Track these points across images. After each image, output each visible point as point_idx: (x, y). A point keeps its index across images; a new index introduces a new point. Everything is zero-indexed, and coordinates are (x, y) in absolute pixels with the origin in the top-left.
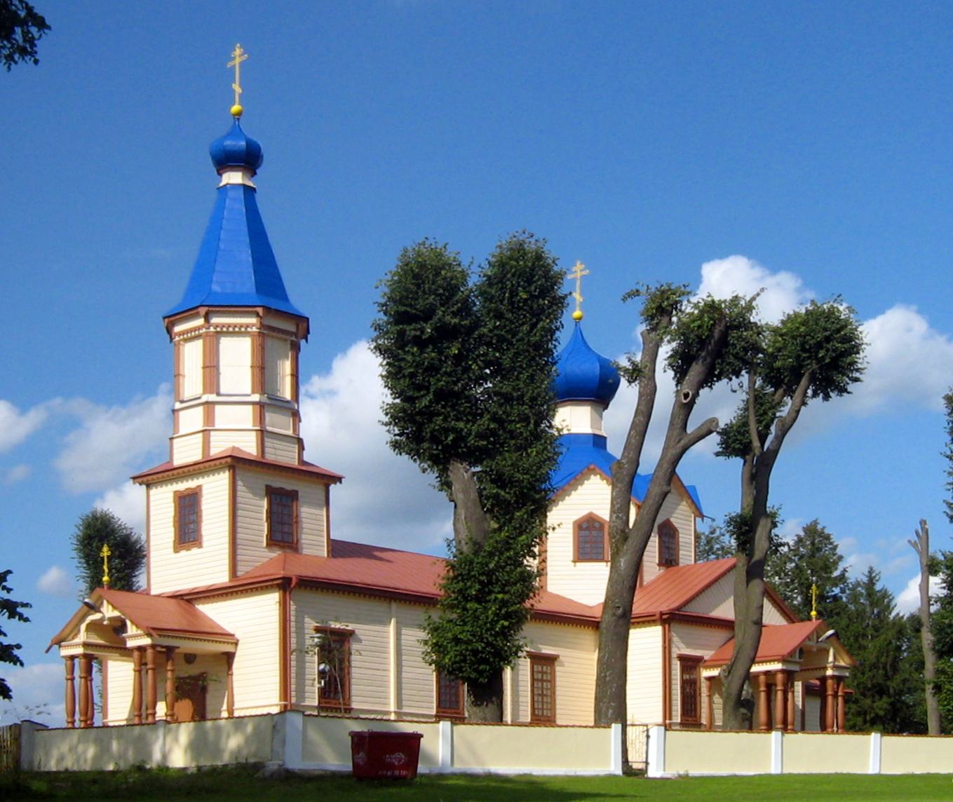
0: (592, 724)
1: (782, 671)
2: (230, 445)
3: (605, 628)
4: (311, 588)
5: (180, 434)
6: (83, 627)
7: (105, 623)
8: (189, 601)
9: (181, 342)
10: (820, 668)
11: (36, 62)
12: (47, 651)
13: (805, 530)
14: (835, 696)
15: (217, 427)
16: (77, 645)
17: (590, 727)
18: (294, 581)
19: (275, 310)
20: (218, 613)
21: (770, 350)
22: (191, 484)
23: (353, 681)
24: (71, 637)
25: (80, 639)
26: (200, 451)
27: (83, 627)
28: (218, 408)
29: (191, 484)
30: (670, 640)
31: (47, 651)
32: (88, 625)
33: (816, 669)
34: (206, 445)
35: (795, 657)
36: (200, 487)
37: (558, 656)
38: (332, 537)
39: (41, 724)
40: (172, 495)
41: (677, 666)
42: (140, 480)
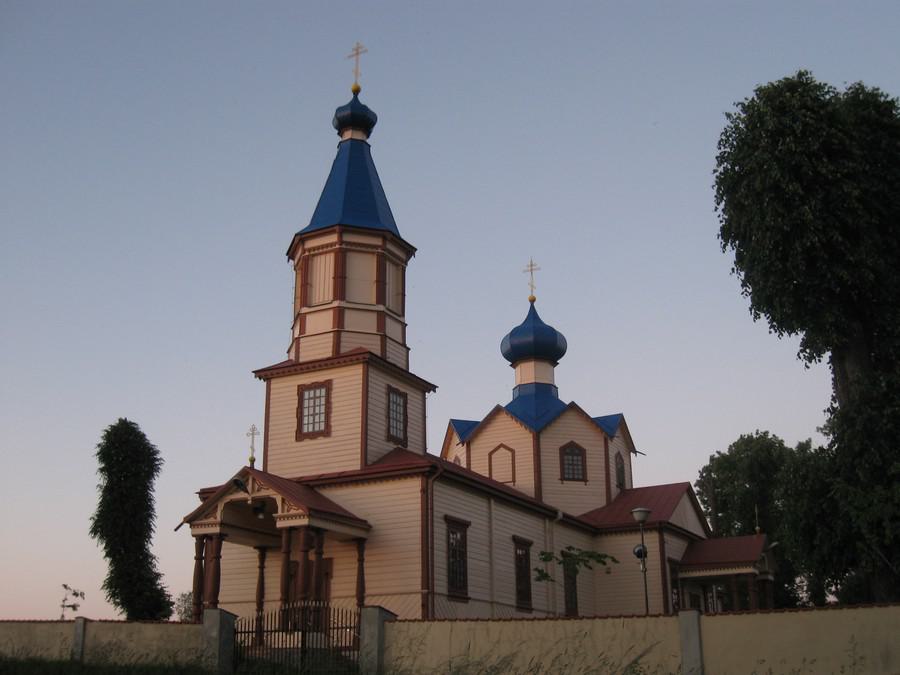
0: (419, 615)
1: (308, 528)
2: (358, 346)
5: (307, 334)
6: (221, 507)
8: (312, 488)
11: (356, 92)
12: (176, 530)
13: (893, 101)
15: (332, 334)
16: (213, 525)
17: (419, 621)
18: (560, 516)
20: (352, 499)
24: (203, 515)
25: (216, 518)
27: (221, 507)
28: (308, 317)
30: (451, 439)
31: (176, 530)
32: (226, 504)
37: (470, 523)
38: (668, 555)
39: (680, 528)
41: (440, 529)
42: (262, 374)
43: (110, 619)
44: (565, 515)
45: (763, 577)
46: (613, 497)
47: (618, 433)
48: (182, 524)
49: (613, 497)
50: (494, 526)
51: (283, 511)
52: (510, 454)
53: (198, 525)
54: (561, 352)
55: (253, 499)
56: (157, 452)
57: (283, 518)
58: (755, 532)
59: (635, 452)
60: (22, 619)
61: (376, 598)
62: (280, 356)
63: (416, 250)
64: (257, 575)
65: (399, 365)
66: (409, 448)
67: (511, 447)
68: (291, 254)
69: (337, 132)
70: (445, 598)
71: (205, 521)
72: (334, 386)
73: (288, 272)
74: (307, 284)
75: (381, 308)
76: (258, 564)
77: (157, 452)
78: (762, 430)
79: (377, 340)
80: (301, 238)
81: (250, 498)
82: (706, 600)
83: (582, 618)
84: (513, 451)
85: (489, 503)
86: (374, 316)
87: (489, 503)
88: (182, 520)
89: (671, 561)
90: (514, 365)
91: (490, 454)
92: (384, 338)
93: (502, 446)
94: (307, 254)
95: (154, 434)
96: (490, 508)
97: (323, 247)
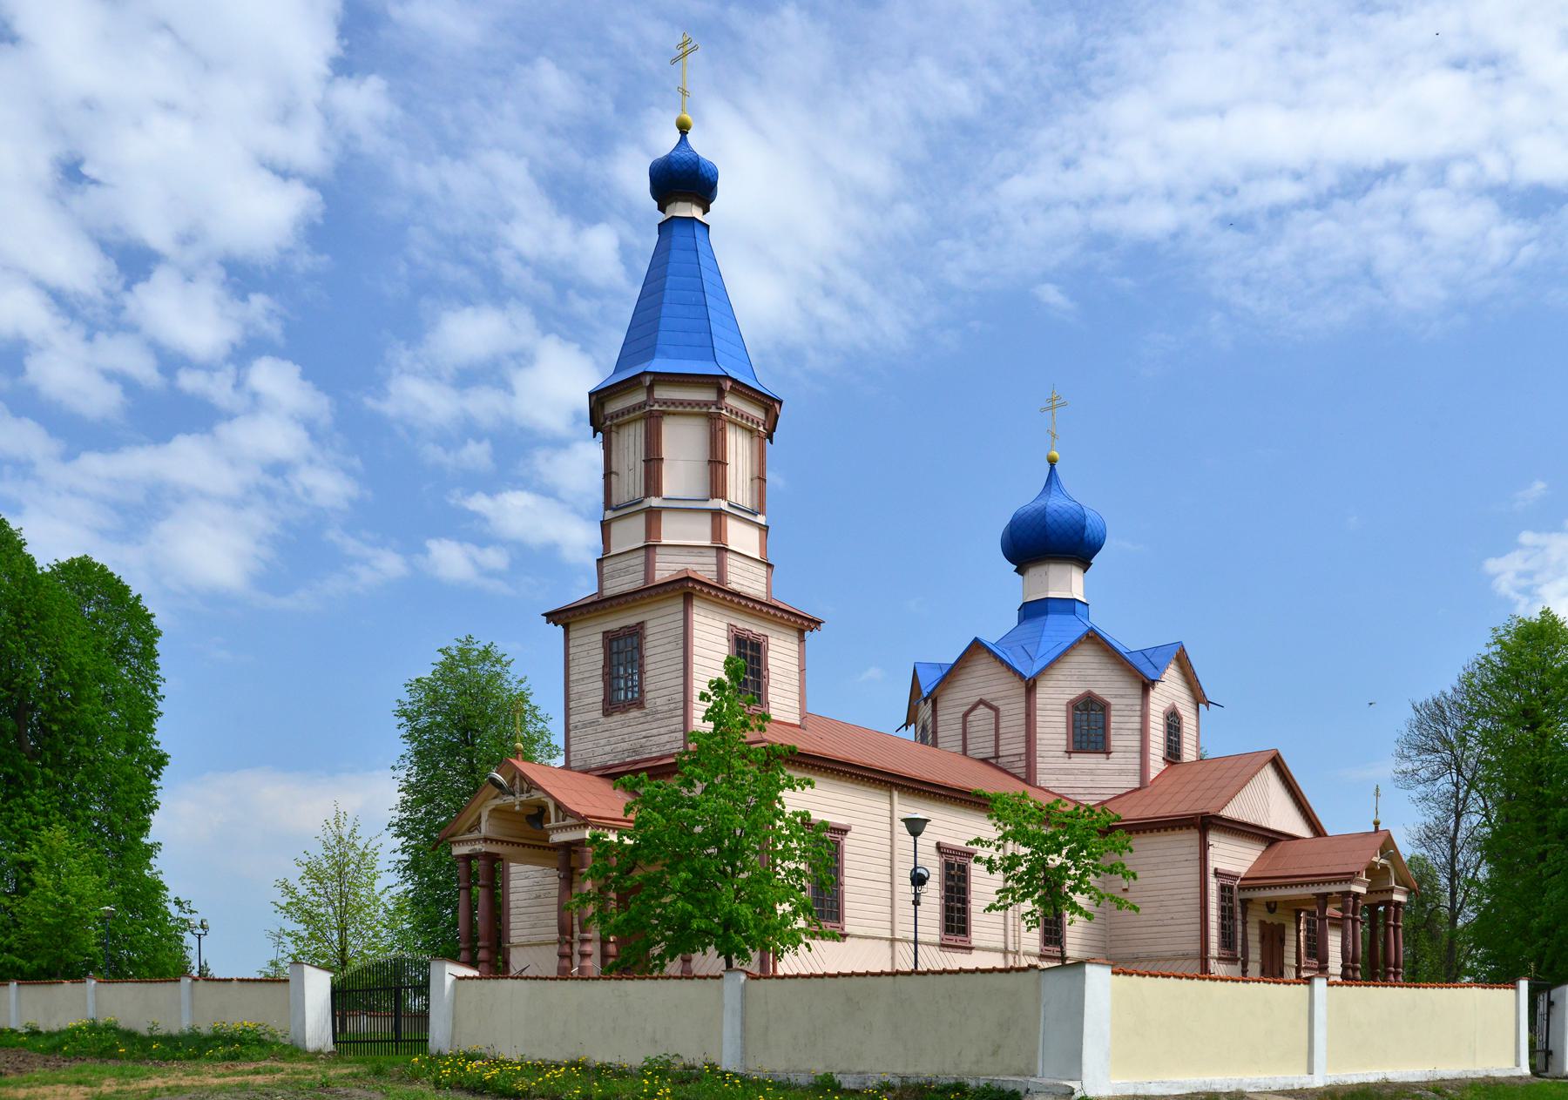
2: (680, 567)
3: (51, 727)
4: (1281, 778)
5: (612, 554)
7: (517, 808)
9: (613, 428)
10: (1387, 891)
14: (1396, 928)
15: (664, 542)
19: (238, 980)
21: (52, 876)
22: (629, 619)
23: (847, 897)
26: (641, 575)
28: (665, 517)
29: (629, 619)
33: (1382, 891)
34: (649, 567)
35: (1362, 876)
36: (641, 625)
40: (600, 637)
42: (556, 618)
43: (252, 978)
46: (1153, 774)
48: (915, 841)
49: (1153, 774)
51: (557, 821)
54: (1095, 547)
55: (522, 803)
57: (557, 829)
59: (1208, 703)
61: (1161, 963)
62: (583, 589)
70: (937, 948)
74: (611, 473)
79: (710, 559)
81: (517, 803)
82: (1244, 923)
83: (1215, 979)
84: (996, 710)
85: (891, 798)
86: (708, 518)
87: (891, 798)
90: (1020, 571)
91: (966, 715)
92: (722, 550)
93: (981, 702)
96: (891, 804)
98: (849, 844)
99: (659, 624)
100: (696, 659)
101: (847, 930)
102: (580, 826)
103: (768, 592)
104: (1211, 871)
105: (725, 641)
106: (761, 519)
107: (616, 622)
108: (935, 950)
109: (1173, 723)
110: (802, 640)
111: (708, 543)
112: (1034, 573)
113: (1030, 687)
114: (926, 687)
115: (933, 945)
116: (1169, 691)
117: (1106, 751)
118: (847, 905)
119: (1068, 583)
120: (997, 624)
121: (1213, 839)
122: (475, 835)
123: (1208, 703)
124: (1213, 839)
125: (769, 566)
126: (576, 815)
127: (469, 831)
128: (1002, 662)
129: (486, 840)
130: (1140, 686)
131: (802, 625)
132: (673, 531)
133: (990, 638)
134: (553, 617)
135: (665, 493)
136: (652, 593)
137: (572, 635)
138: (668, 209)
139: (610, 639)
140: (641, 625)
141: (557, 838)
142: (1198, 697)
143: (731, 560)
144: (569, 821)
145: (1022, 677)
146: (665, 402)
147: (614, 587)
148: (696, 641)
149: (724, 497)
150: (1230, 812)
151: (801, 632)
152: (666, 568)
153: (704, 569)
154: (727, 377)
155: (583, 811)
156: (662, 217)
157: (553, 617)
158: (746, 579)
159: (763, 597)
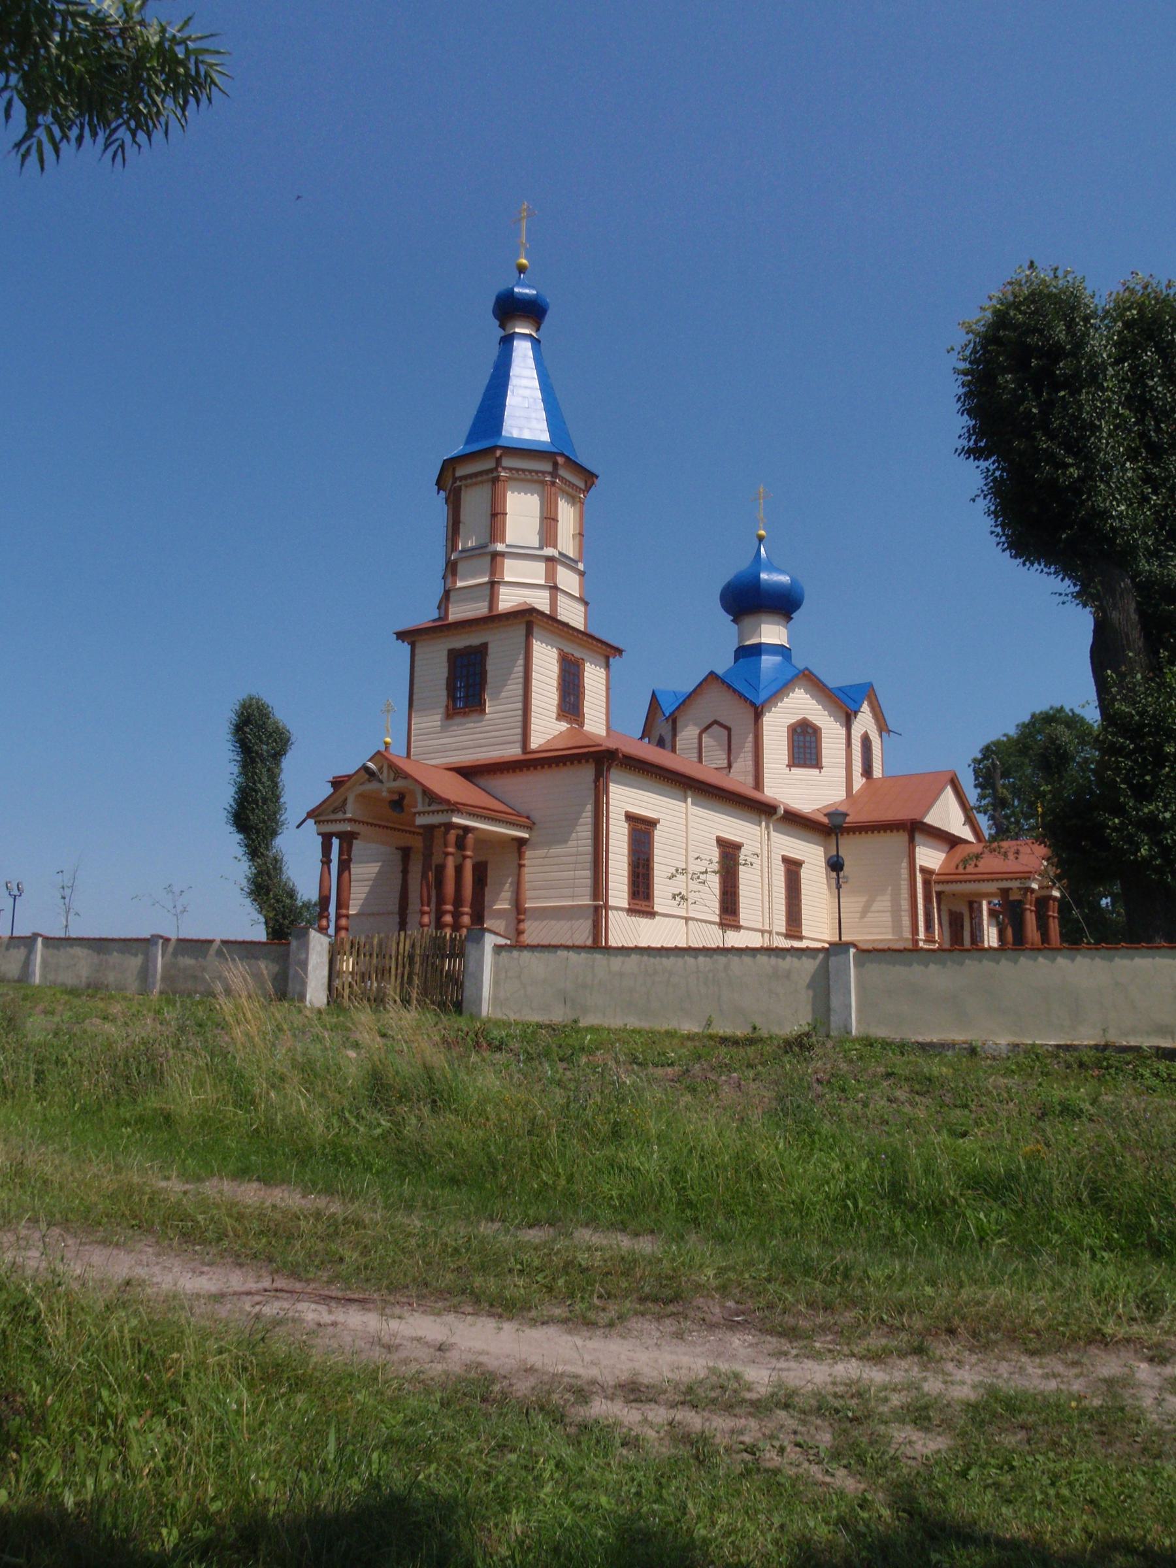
2: (522, 600)
12: (298, 827)
15: (506, 579)
31: (298, 827)
34: (493, 599)
40: (445, 653)
44: (787, 812)
45: (1044, 893)
47: (865, 707)
50: (773, 844)
52: (726, 732)
53: (323, 822)
56: (1061, 709)
58: (370, 760)
60: (129, 936)
62: (424, 615)
63: (597, 477)
64: (399, 882)
65: (573, 624)
66: (586, 727)
67: (728, 724)
68: (440, 484)
69: (497, 323)
71: (333, 817)
72: (490, 651)
73: (438, 503)
75: (549, 551)
76: (400, 868)
77: (1061, 709)
78: (1057, 705)
80: (450, 464)
84: (729, 729)
88: (305, 815)
89: (924, 870)
94: (458, 483)
95: (283, 714)
97: (476, 475)
98: (659, 835)
99: (500, 646)
100: (534, 675)
101: (656, 909)
102: (447, 811)
103: (586, 625)
104: (918, 867)
105: (555, 662)
106: (581, 566)
107: (461, 641)
108: (623, 914)
109: (866, 742)
110: (607, 666)
111: (542, 582)
112: (748, 621)
113: (758, 715)
114: (668, 708)
115: (621, 909)
116: (864, 722)
117: (790, 766)
118: (656, 886)
119: (772, 633)
120: (723, 663)
121: (918, 838)
122: (340, 816)
123: (889, 731)
124: (918, 838)
125: (586, 604)
126: (448, 802)
127: (334, 811)
128: (735, 691)
129: (350, 820)
130: (844, 716)
131: (608, 652)
132: (512, 570)
133: (720, 671)
134: (401, 636)
135: (508, 541)
136: (495, 620)
137: (417, 651)
138: (509, 326)
139: (455, 657)
140: (485, 646)
141: (420, 821)
142: (883, 727)
143: (561, 598)
144: (434, 808)
145: (753, 704)
146: (511, 469)
147: (456, 613)
148: (535, 660)
149: (555, 546)
150: (930, 819)
151: (607, 658)
152: (508, 600)
153: (541, 600)
154: (562, 455)
155: (453, 797)
156: (502, 333)
157: (401, 636)
158: (572, 614)
159: (582, 628)
